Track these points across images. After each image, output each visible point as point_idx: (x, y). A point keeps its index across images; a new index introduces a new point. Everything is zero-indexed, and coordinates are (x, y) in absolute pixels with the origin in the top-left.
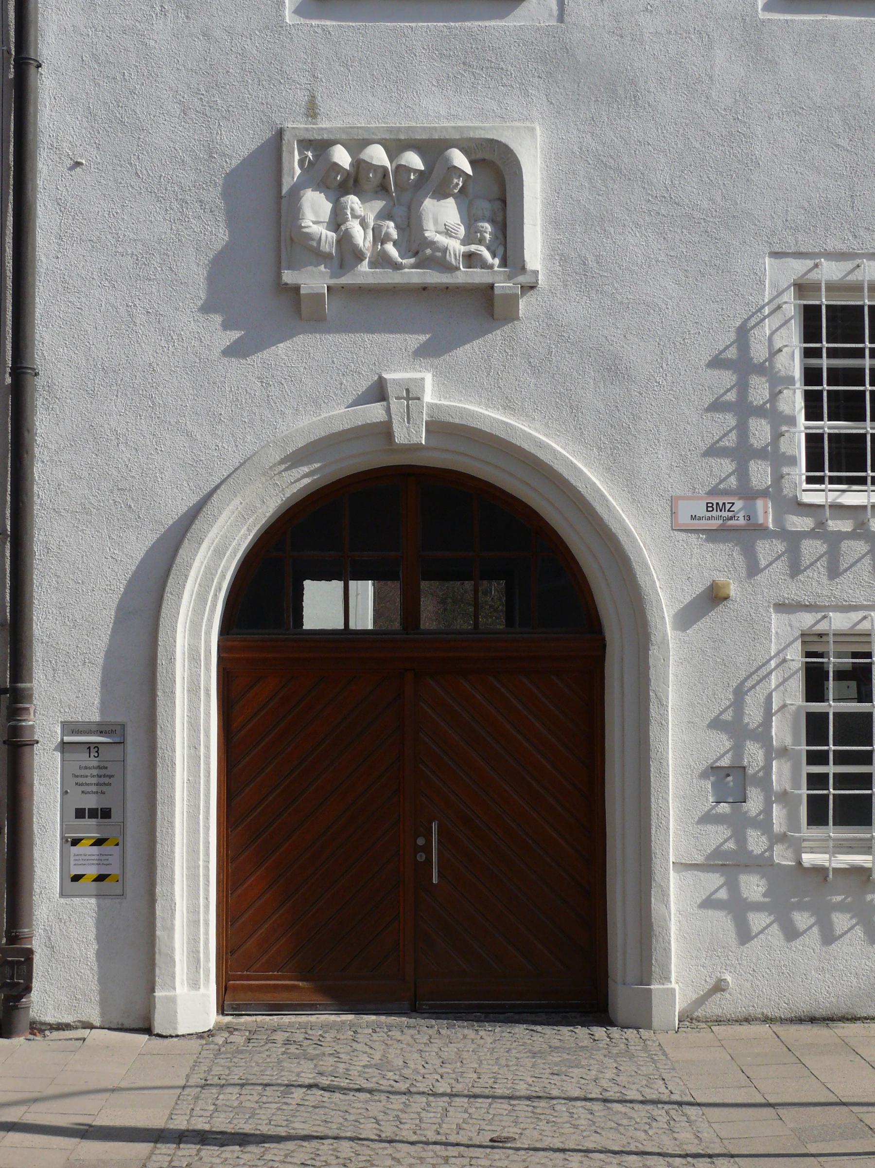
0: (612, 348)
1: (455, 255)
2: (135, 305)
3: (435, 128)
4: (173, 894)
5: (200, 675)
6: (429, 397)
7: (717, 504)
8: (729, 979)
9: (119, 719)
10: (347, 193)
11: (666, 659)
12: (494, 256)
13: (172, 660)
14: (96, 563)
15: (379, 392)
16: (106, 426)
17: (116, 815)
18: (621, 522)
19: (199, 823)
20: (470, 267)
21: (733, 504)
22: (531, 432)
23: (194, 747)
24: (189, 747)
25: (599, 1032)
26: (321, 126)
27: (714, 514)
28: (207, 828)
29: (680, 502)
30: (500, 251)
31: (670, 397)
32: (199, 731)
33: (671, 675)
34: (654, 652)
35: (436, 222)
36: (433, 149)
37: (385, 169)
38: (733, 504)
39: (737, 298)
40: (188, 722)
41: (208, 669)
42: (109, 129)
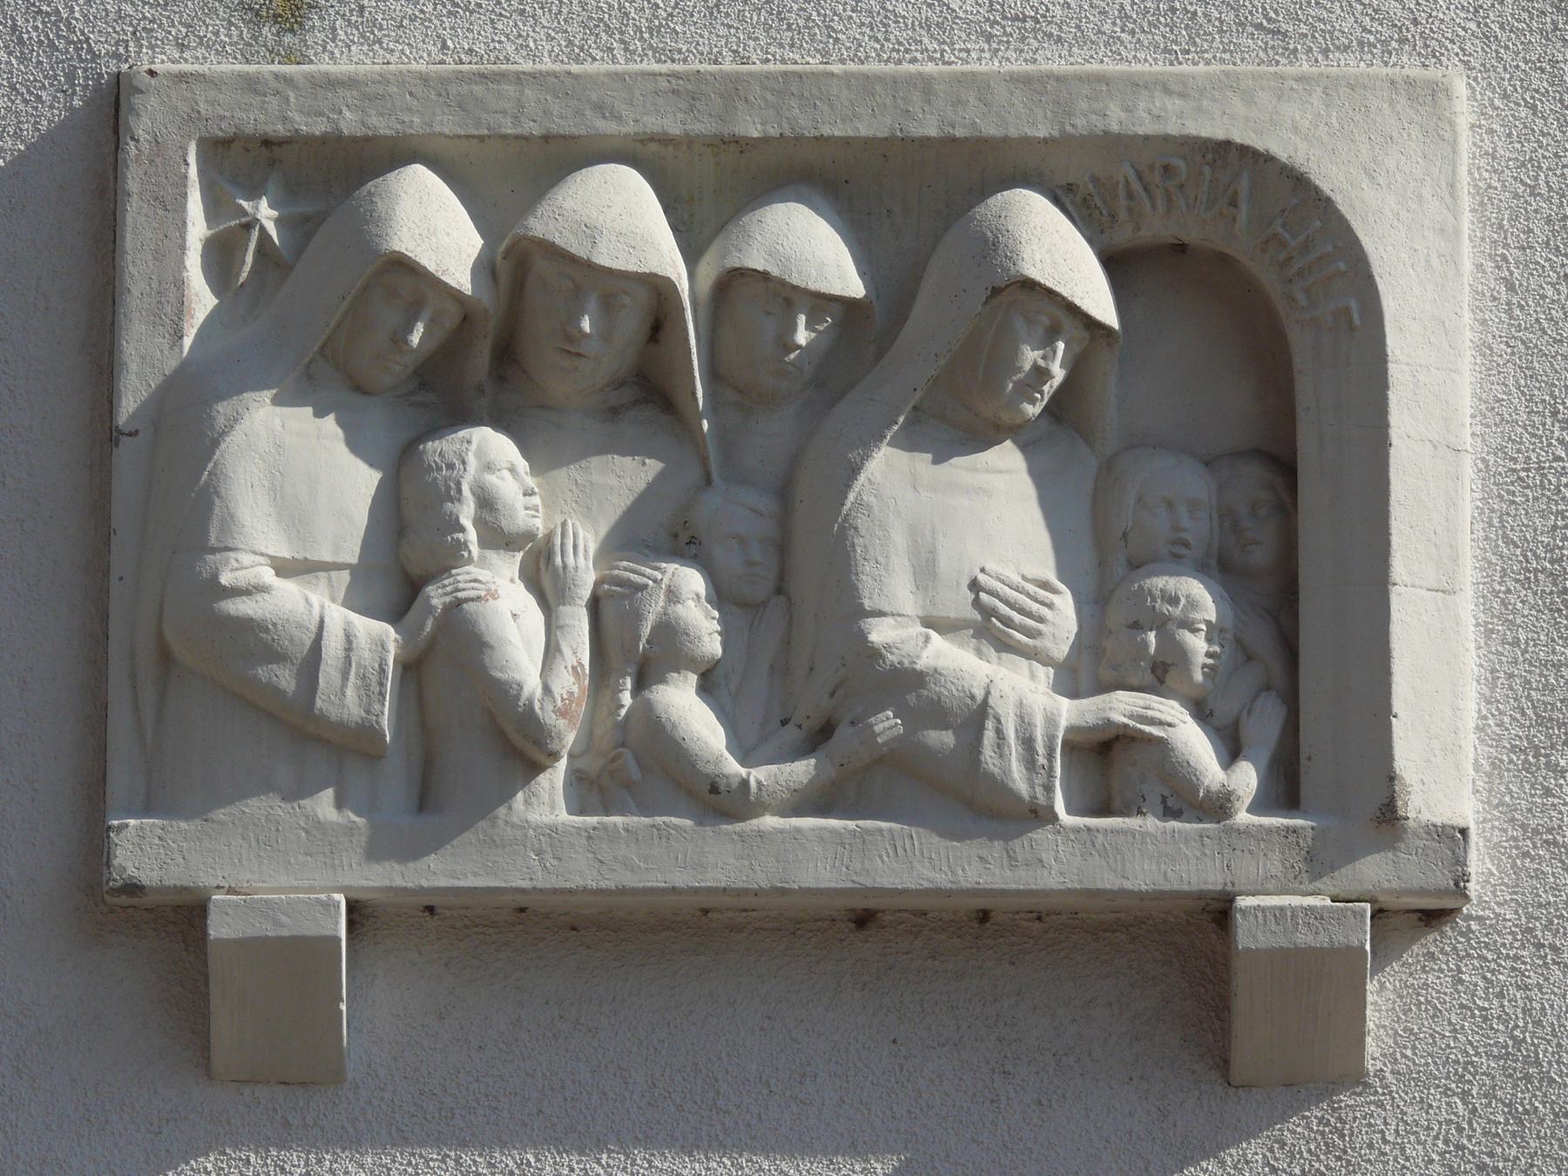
1: (1028, 743)
12: (1231, 751)
26: (325, 66)
30: (1265, 725)
35: (926, 571)
36: (915, 192)
37: (658, 290)
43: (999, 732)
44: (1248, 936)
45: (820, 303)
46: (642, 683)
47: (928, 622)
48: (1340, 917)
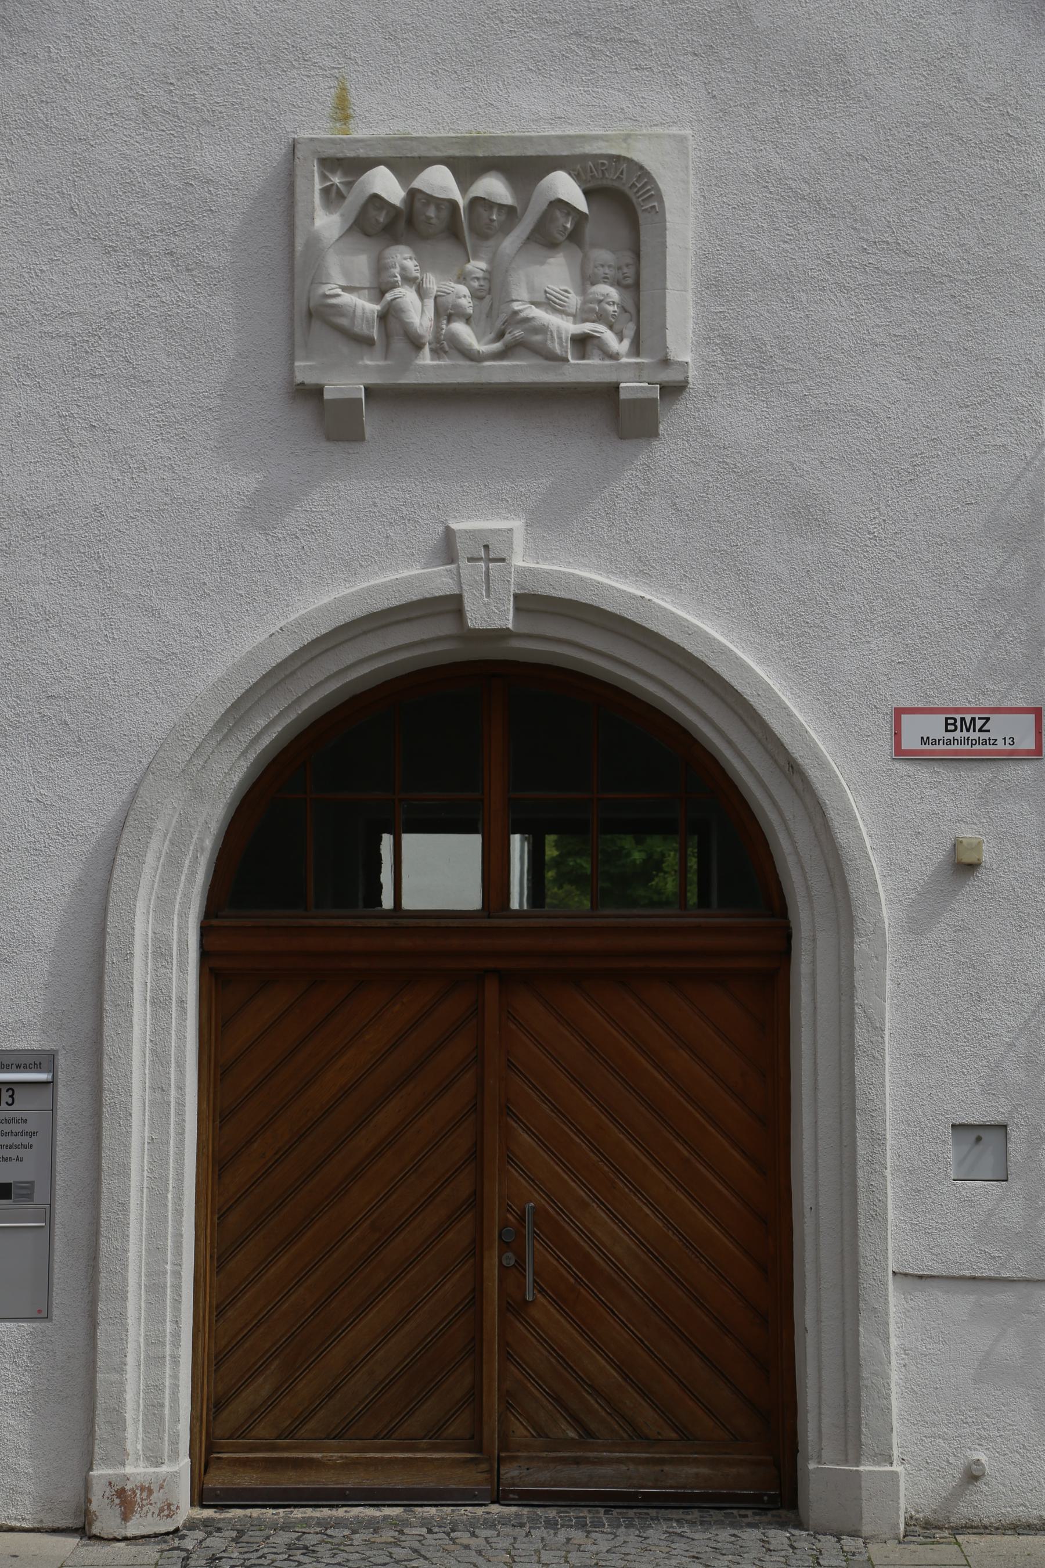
0: (800, 480)
1: (560, 338)
2: (72, 415)
3: (530, 139)
4: (123, 1315)
5: (170, 979)
6: (519, 560)
7: (963, 719)
8: (984, 1459)
9: (48, 1046)
10: (396, 240)
11: (881, 956)
12: (621, 338)
13: (128, 957)
14: (13, 809)
15: (448, 548)
16: (28, 600)
17: (40, 1195)
18: (811, 746)
19: (166, 1205)
20: (583, 358)
21: (988, 719)
22: (674, 610)
23: (160, 1088)
24: (152, 1088)
25: (779, 1537)
26: (355, 135)
27: (958, 734)
28: (179, 1212)
29: (905, 718)
30: (630, 330)
31: (891, 555)
32: (168, 1063)
33: (888, 982)
34: (862, 946)
35: (531, 289)
36: (525, 169)
37: (453, 204)
38: (988, 719)
39: (999, 401)
40: (152, 1050)
41: (182, 970)
42: (27, 138)
43: (552, 335)
44: (623, 396)
45: (501, 206)
46: (449, 321)
47: (532, 303)
48: (651, 389)
